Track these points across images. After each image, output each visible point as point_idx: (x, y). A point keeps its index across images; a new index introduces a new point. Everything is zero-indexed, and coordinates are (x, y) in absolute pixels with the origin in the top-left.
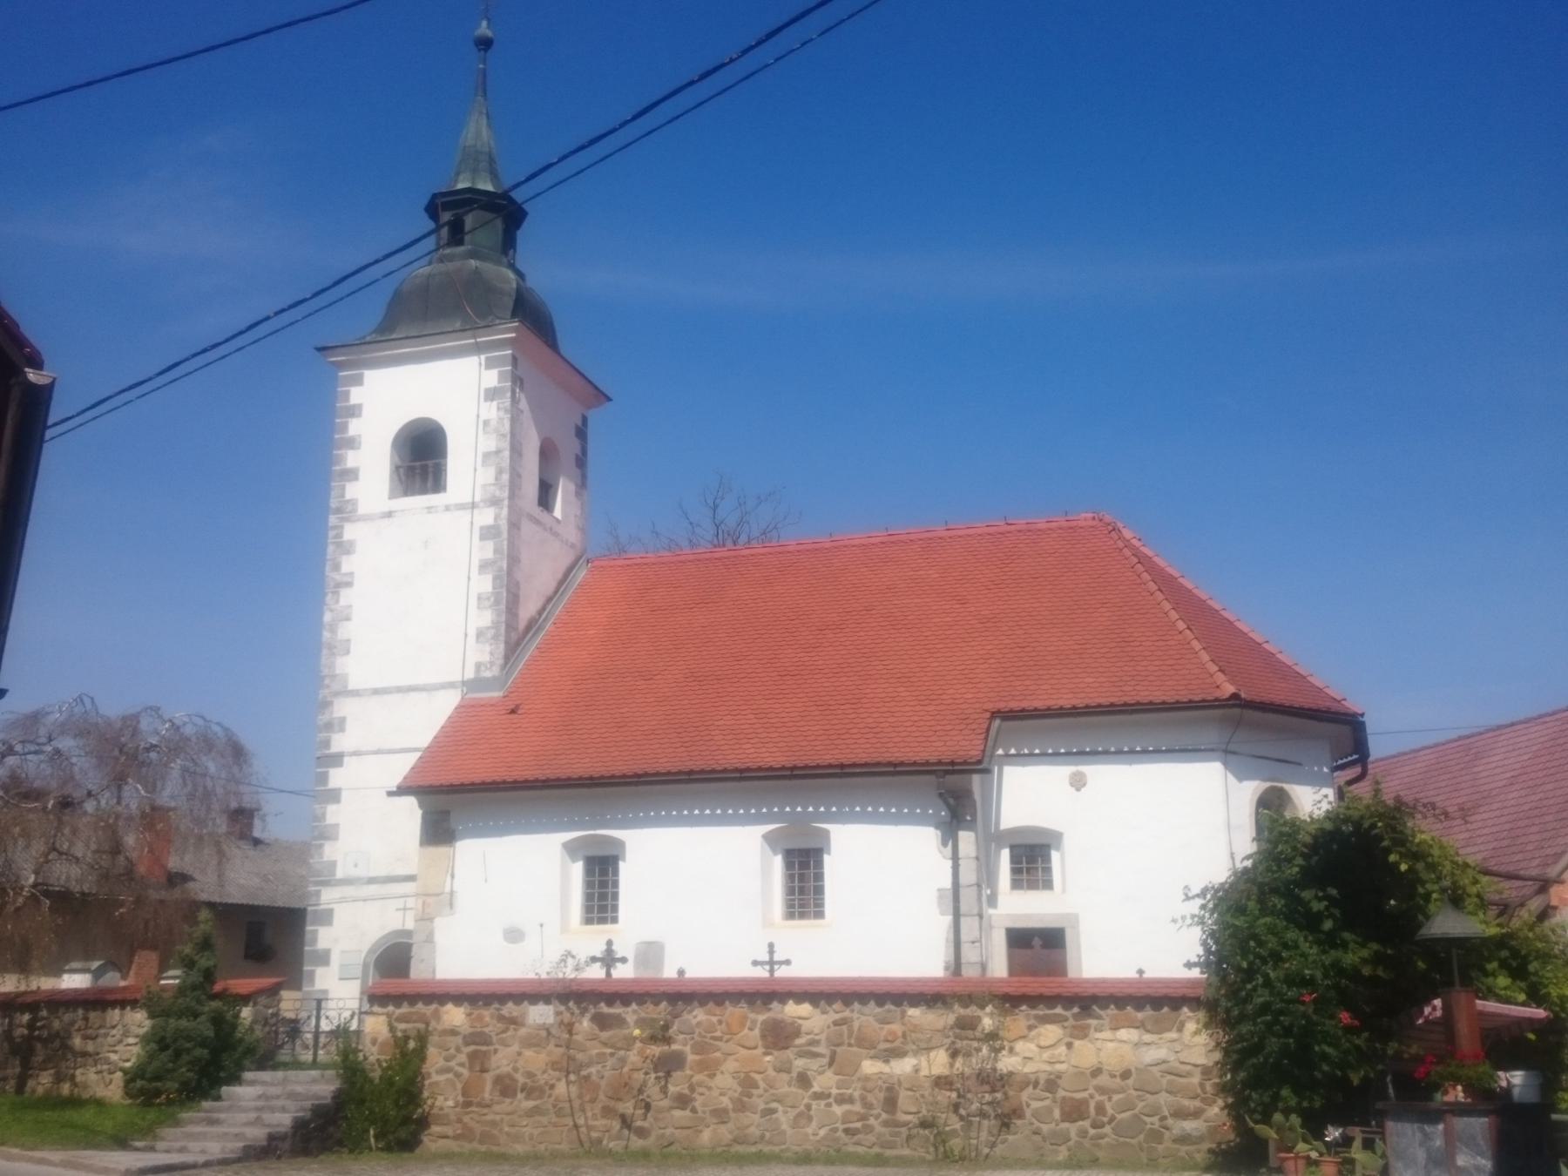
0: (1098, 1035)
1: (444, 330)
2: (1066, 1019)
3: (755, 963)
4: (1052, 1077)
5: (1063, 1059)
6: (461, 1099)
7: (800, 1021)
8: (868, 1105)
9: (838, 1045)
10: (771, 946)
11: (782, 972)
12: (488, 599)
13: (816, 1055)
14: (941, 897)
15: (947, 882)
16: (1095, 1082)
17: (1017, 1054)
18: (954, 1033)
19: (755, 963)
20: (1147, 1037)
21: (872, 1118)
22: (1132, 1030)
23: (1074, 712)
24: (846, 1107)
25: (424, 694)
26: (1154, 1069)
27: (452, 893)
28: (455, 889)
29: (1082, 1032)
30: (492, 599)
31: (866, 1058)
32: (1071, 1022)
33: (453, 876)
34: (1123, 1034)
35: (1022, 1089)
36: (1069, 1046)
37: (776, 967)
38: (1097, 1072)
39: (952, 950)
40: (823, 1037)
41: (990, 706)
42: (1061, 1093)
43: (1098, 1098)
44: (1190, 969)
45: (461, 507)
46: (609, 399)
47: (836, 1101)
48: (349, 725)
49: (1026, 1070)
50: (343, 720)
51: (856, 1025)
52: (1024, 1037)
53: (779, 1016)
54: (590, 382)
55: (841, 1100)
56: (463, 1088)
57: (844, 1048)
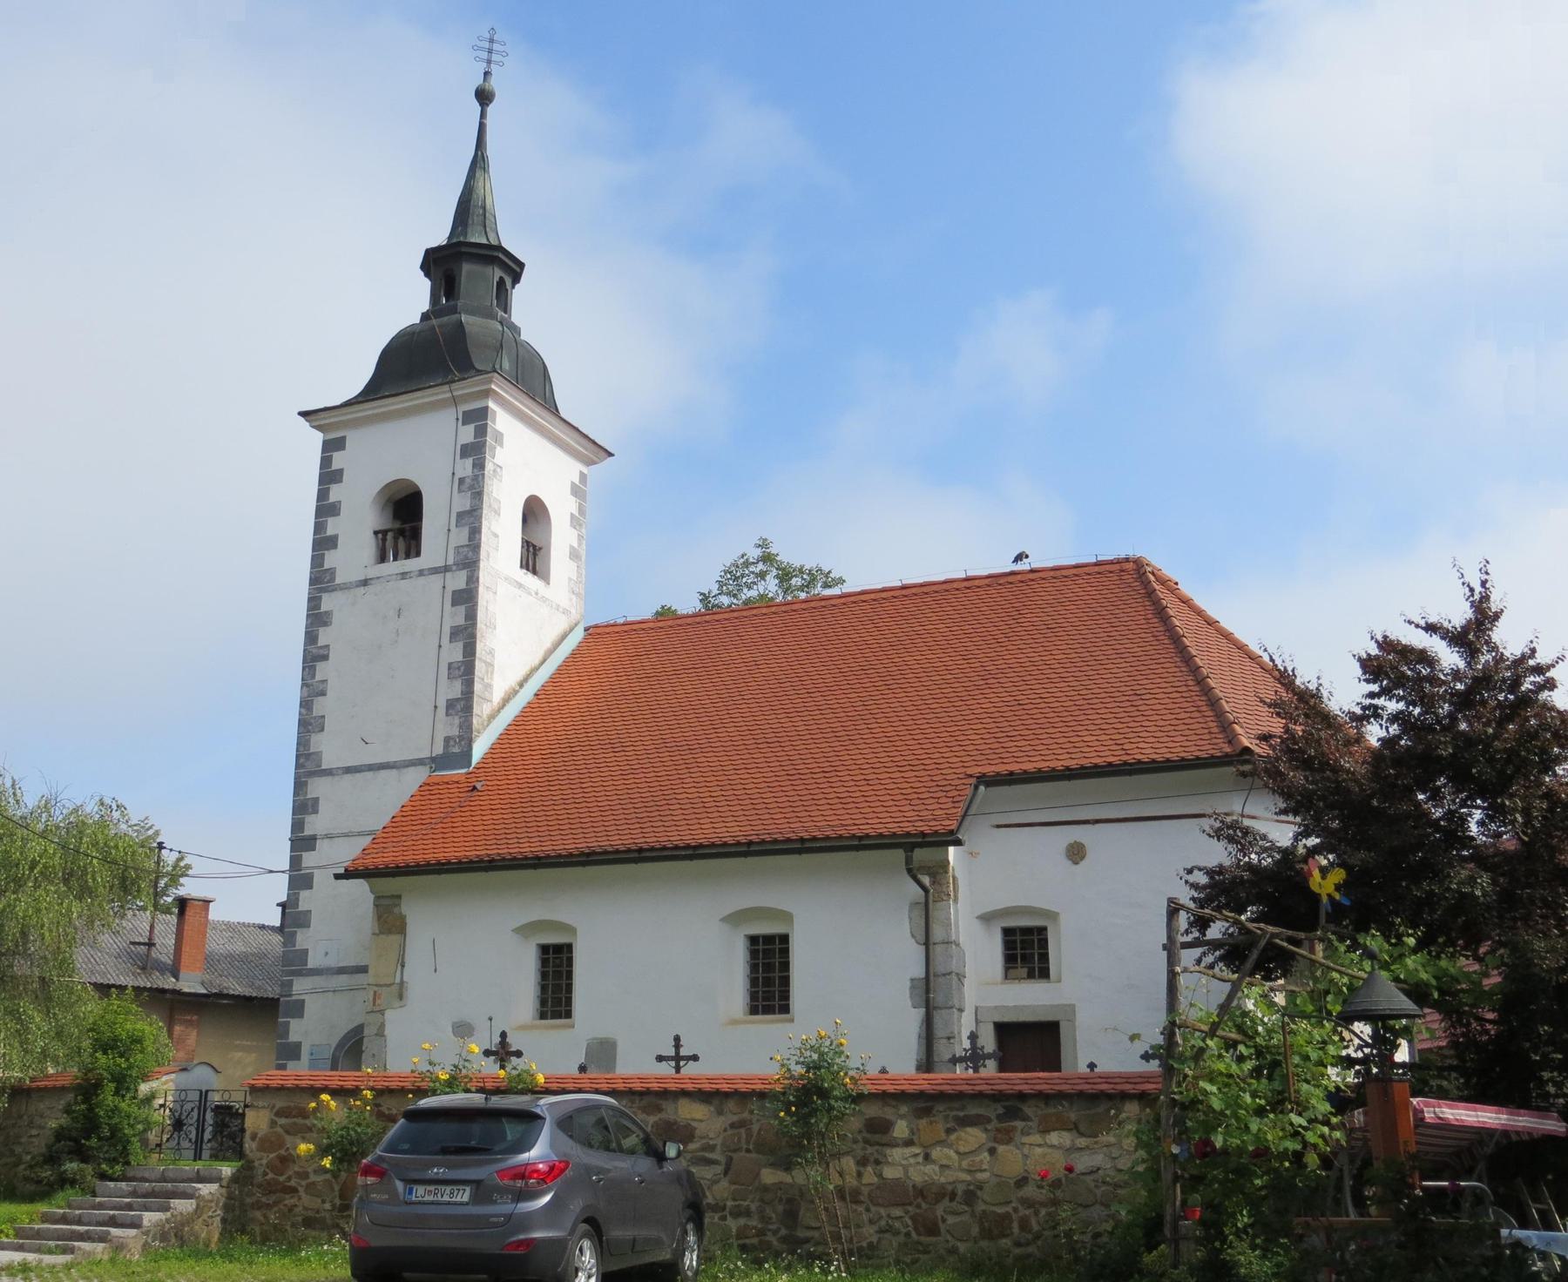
0: (1026, 1139)
1: (410, 389)
2: (989, 1120)
3: (660, 1059)
4: (972, 1187)
5: (984, 1167)
6: (338, 1202)
7: (694, 1124)
8: (765, 1219)
9: (735, 1151)
10: (677, 1039)
11: (689, 1069)
12: (459, 668)
13: (710, 1162)
14: (913, 987)
15: (920, 972)
16: (1021, 1193)
17: (934, 1162)
18: (863, 1138)
19: (660, 1059)
20: (1082, 1142)
21: (769, 1233)
22: (1065, 1134)
23: (1069, 774)
24: (742, 1221)
25: (394, 771)
26: (1088, 1179)
27: (402, 983)
28: (405, 979)
29: (1006, 1137)
30: (462, 668)
31: (765, 1166)
32: (994, 1124)
33: (403, 966)
34: (1054, 1138)
35: (937, 1202)
36: (992, 1151)
37: (682, 1063)
38: (1022, 1182)
39: (924, 1048)
40: (719, 1142)
41: (976, 771)
42: (980, 1207)
43: (1024, 1212)
44: (1148, 1061)
45: (435, 571)
46: (611, 455)
47: (731, 1214)
48: (322, 806)
49: (943, 1180)
50: (316, 800)
51: (755, 1128)
52: (941, 1143)
53: (672, 1117)
54: (586, 436)
55: (736, 1214)
56: (341, 1190)
57: (743, 1154)
